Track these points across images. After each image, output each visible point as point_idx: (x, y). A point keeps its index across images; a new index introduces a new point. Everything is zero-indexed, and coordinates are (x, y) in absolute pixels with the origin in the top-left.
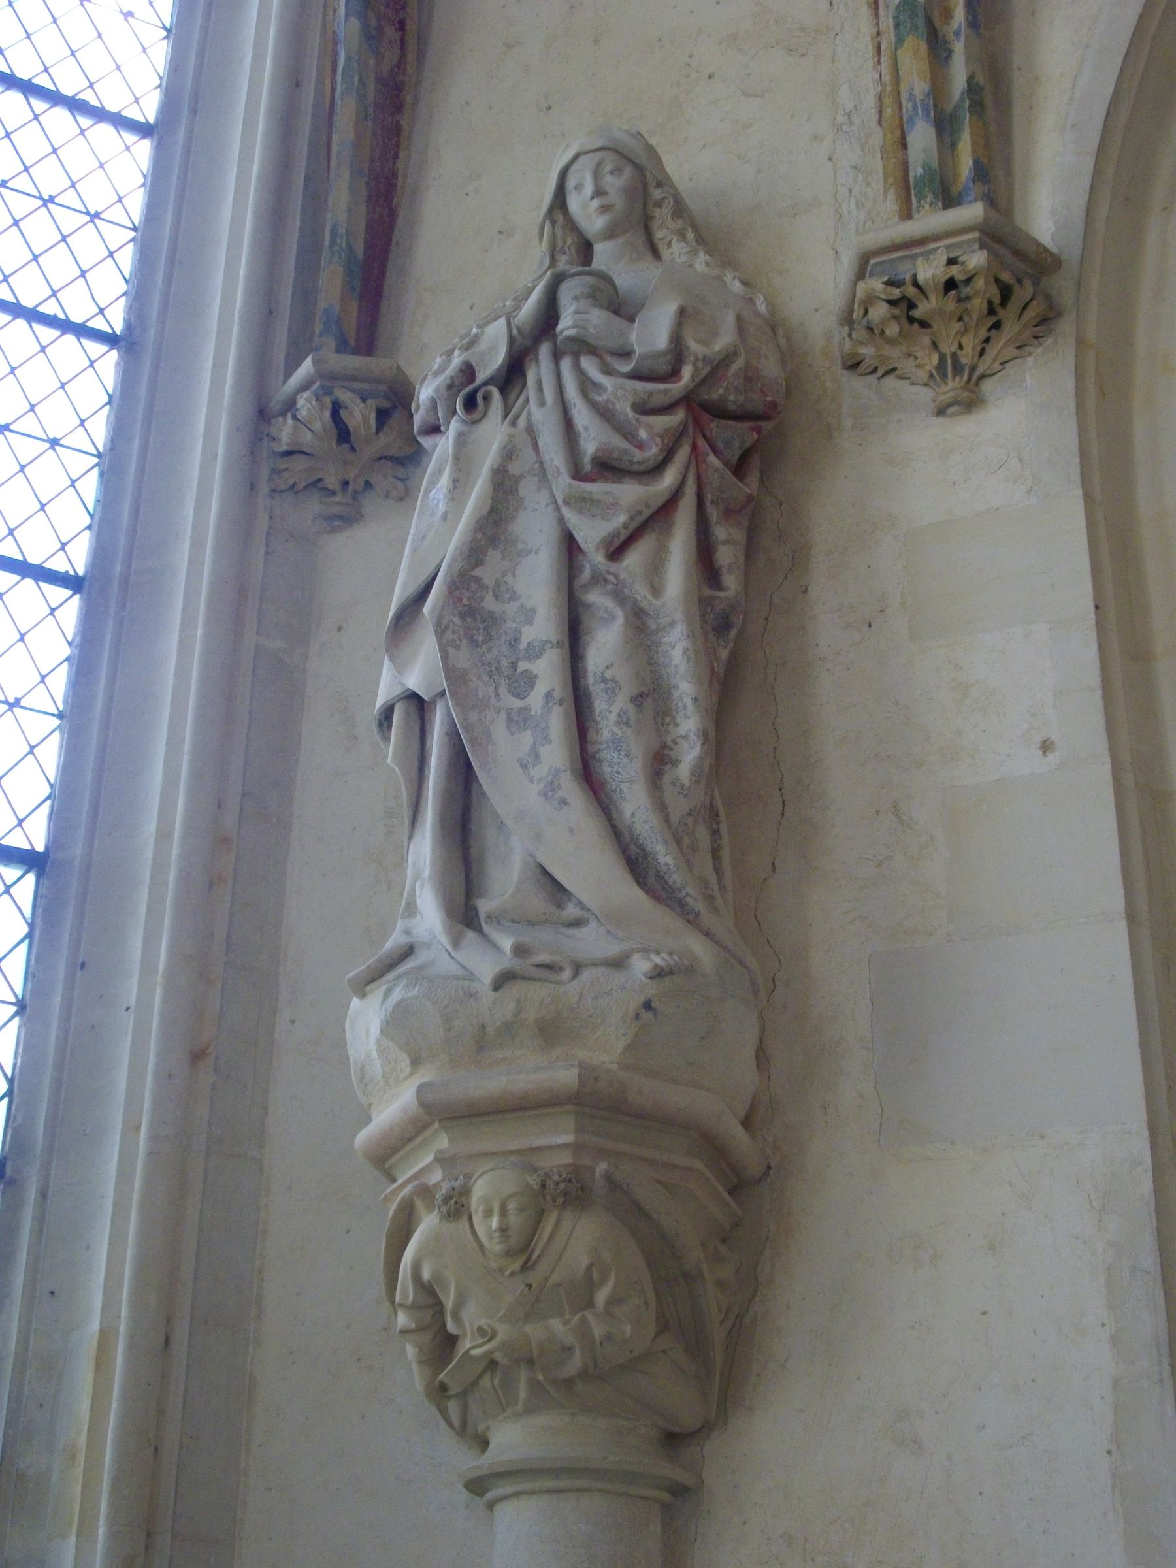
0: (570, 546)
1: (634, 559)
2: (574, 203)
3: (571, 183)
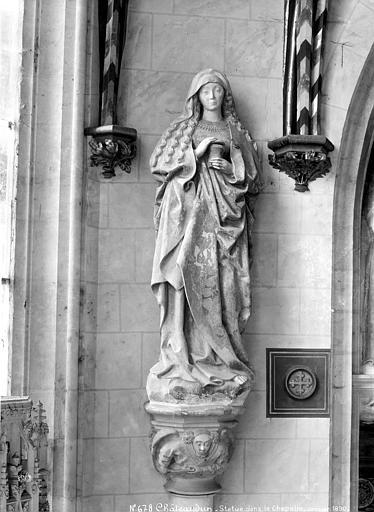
0: (218, 246)
1: (234, 256)
2: (203, 96)
3: (204, 90)
